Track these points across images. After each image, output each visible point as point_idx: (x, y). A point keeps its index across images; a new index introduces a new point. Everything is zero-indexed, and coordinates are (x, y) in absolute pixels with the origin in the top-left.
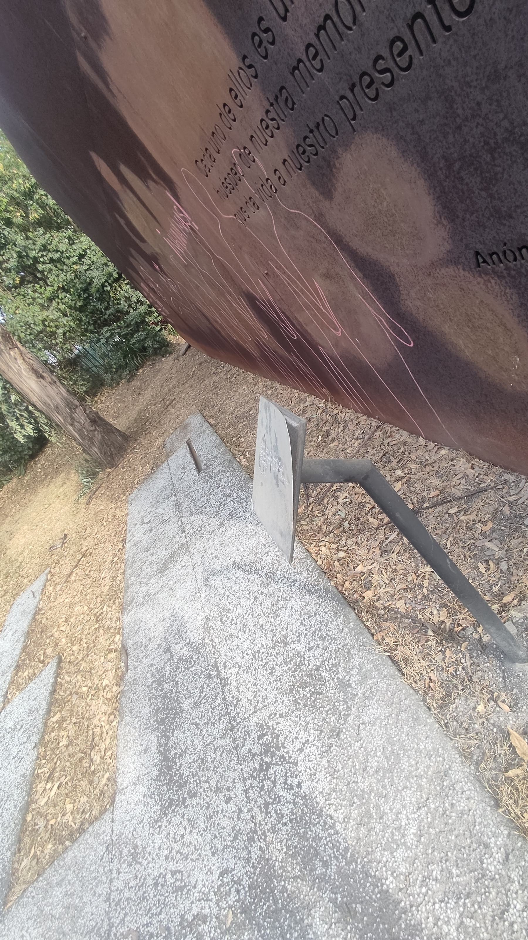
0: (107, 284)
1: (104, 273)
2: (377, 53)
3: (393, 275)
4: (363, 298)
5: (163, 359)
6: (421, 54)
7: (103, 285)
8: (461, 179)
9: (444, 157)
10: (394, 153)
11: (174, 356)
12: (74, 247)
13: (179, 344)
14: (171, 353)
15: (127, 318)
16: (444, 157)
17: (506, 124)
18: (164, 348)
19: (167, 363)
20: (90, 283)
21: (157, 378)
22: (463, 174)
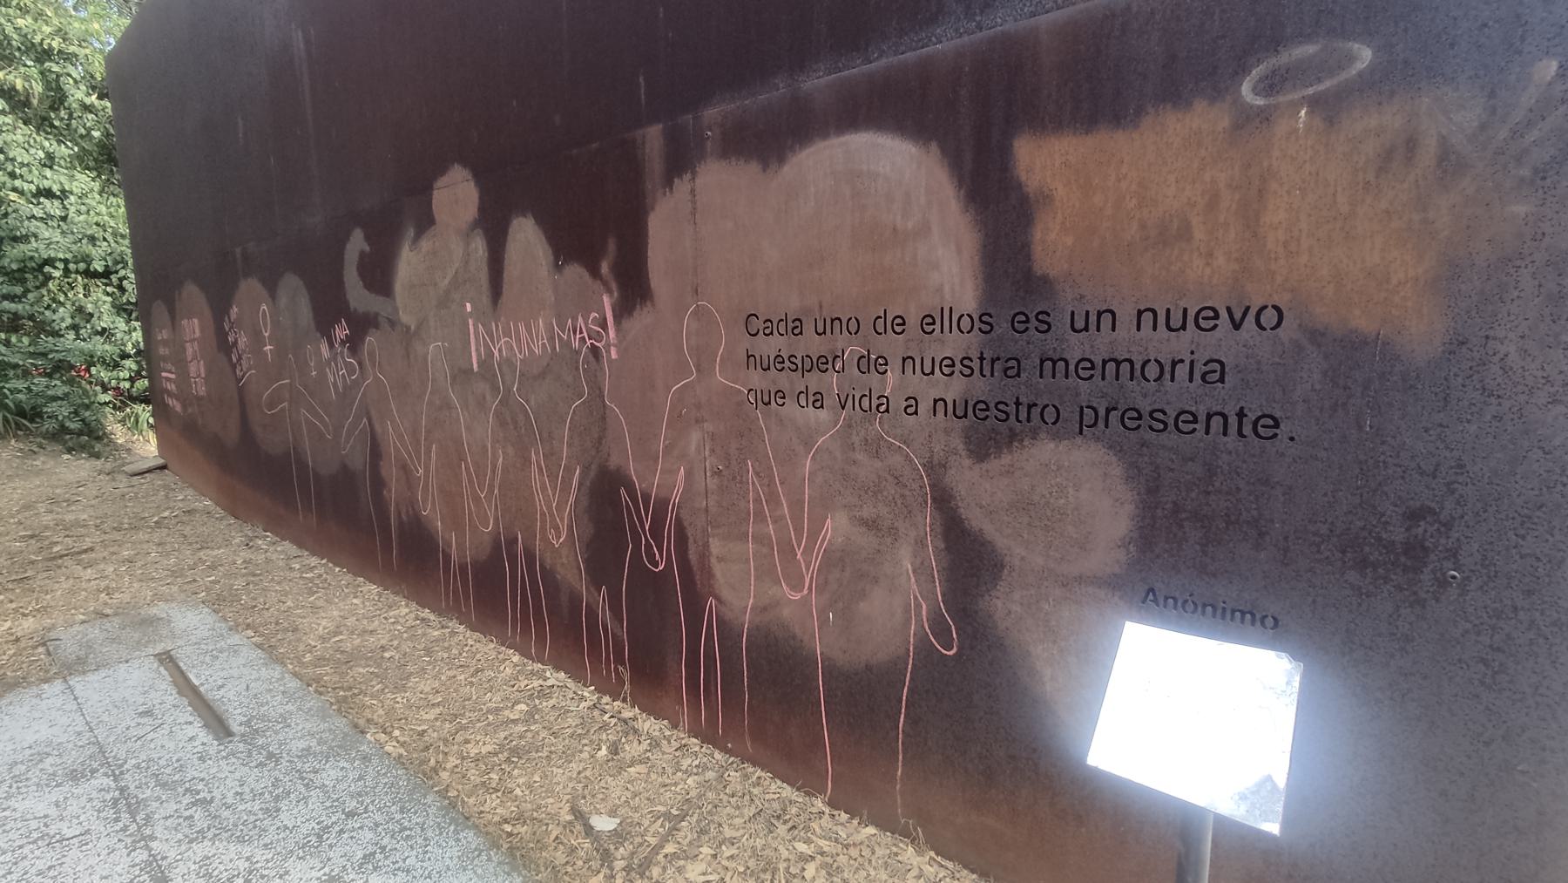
0: (61, 265)
1: (74, 248)
2: (558, 268)
3: (1003, 566)
4: (914, 571)
5: (66, 457)
6: (1207, 433)
7: (50, 262)
8: (1181, 527)
9: (1175, 503)
10: (1117, 471)
11: (99, 463)
12: (48, 173)
13: (129, 450)
14: (97, 456)
15: (47, 342)
16: (1175, 503)
17: (1255, 513)
18: (86, 438)
19: (73, 469)
20: (25, 239)
21: (18, 483)
22: (1186, 524)
